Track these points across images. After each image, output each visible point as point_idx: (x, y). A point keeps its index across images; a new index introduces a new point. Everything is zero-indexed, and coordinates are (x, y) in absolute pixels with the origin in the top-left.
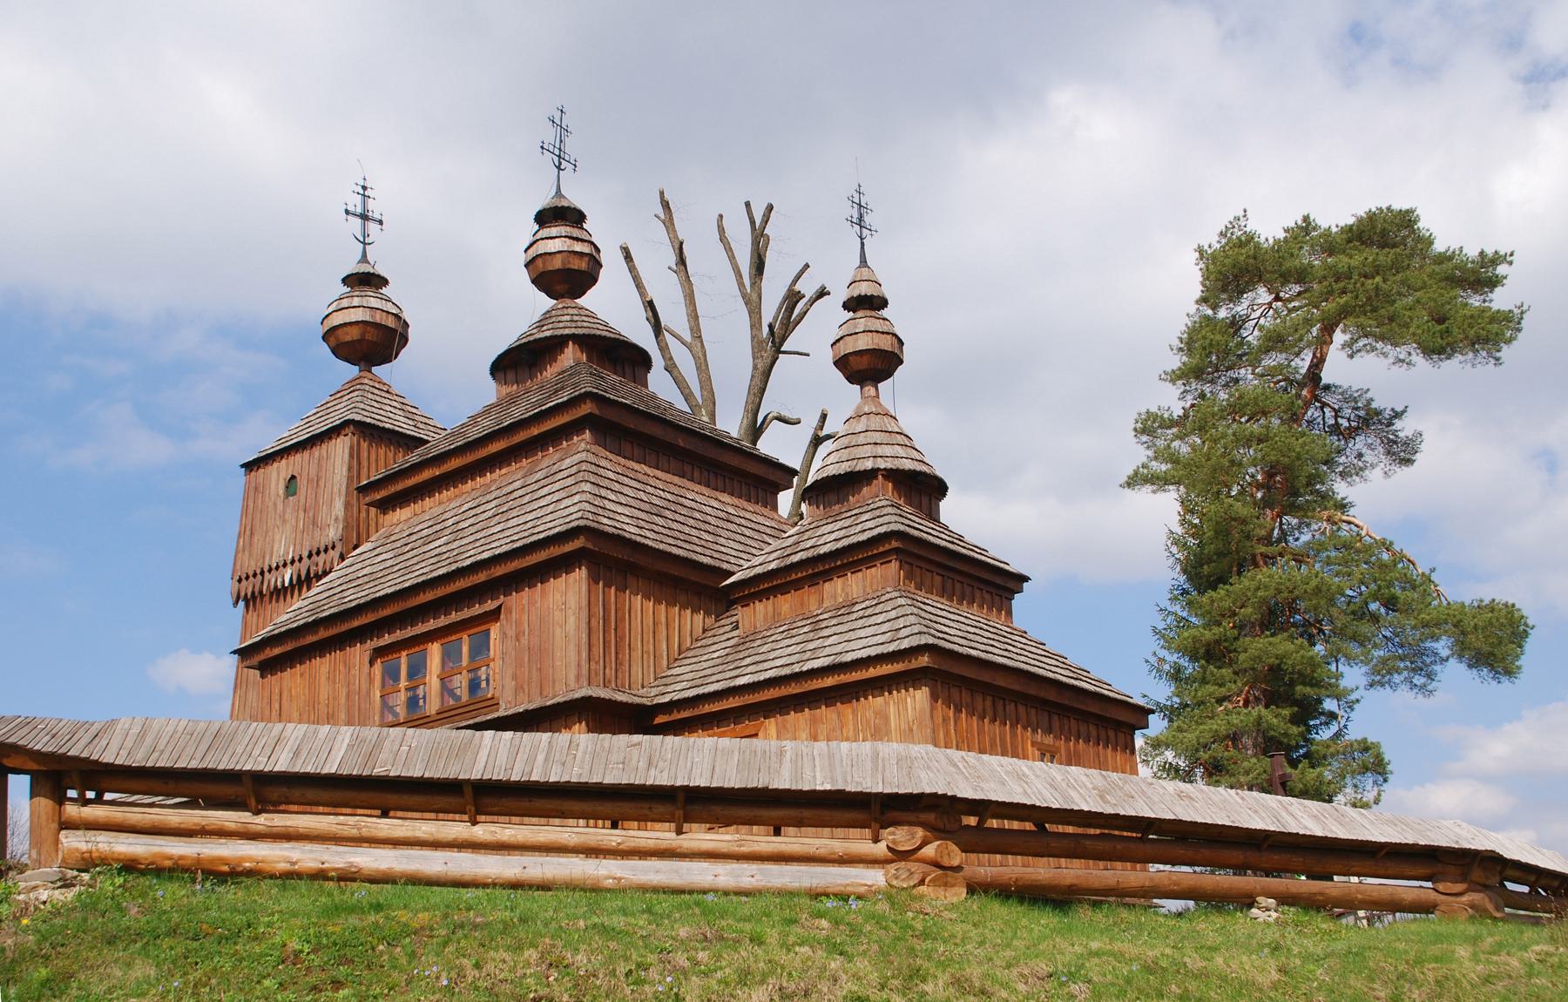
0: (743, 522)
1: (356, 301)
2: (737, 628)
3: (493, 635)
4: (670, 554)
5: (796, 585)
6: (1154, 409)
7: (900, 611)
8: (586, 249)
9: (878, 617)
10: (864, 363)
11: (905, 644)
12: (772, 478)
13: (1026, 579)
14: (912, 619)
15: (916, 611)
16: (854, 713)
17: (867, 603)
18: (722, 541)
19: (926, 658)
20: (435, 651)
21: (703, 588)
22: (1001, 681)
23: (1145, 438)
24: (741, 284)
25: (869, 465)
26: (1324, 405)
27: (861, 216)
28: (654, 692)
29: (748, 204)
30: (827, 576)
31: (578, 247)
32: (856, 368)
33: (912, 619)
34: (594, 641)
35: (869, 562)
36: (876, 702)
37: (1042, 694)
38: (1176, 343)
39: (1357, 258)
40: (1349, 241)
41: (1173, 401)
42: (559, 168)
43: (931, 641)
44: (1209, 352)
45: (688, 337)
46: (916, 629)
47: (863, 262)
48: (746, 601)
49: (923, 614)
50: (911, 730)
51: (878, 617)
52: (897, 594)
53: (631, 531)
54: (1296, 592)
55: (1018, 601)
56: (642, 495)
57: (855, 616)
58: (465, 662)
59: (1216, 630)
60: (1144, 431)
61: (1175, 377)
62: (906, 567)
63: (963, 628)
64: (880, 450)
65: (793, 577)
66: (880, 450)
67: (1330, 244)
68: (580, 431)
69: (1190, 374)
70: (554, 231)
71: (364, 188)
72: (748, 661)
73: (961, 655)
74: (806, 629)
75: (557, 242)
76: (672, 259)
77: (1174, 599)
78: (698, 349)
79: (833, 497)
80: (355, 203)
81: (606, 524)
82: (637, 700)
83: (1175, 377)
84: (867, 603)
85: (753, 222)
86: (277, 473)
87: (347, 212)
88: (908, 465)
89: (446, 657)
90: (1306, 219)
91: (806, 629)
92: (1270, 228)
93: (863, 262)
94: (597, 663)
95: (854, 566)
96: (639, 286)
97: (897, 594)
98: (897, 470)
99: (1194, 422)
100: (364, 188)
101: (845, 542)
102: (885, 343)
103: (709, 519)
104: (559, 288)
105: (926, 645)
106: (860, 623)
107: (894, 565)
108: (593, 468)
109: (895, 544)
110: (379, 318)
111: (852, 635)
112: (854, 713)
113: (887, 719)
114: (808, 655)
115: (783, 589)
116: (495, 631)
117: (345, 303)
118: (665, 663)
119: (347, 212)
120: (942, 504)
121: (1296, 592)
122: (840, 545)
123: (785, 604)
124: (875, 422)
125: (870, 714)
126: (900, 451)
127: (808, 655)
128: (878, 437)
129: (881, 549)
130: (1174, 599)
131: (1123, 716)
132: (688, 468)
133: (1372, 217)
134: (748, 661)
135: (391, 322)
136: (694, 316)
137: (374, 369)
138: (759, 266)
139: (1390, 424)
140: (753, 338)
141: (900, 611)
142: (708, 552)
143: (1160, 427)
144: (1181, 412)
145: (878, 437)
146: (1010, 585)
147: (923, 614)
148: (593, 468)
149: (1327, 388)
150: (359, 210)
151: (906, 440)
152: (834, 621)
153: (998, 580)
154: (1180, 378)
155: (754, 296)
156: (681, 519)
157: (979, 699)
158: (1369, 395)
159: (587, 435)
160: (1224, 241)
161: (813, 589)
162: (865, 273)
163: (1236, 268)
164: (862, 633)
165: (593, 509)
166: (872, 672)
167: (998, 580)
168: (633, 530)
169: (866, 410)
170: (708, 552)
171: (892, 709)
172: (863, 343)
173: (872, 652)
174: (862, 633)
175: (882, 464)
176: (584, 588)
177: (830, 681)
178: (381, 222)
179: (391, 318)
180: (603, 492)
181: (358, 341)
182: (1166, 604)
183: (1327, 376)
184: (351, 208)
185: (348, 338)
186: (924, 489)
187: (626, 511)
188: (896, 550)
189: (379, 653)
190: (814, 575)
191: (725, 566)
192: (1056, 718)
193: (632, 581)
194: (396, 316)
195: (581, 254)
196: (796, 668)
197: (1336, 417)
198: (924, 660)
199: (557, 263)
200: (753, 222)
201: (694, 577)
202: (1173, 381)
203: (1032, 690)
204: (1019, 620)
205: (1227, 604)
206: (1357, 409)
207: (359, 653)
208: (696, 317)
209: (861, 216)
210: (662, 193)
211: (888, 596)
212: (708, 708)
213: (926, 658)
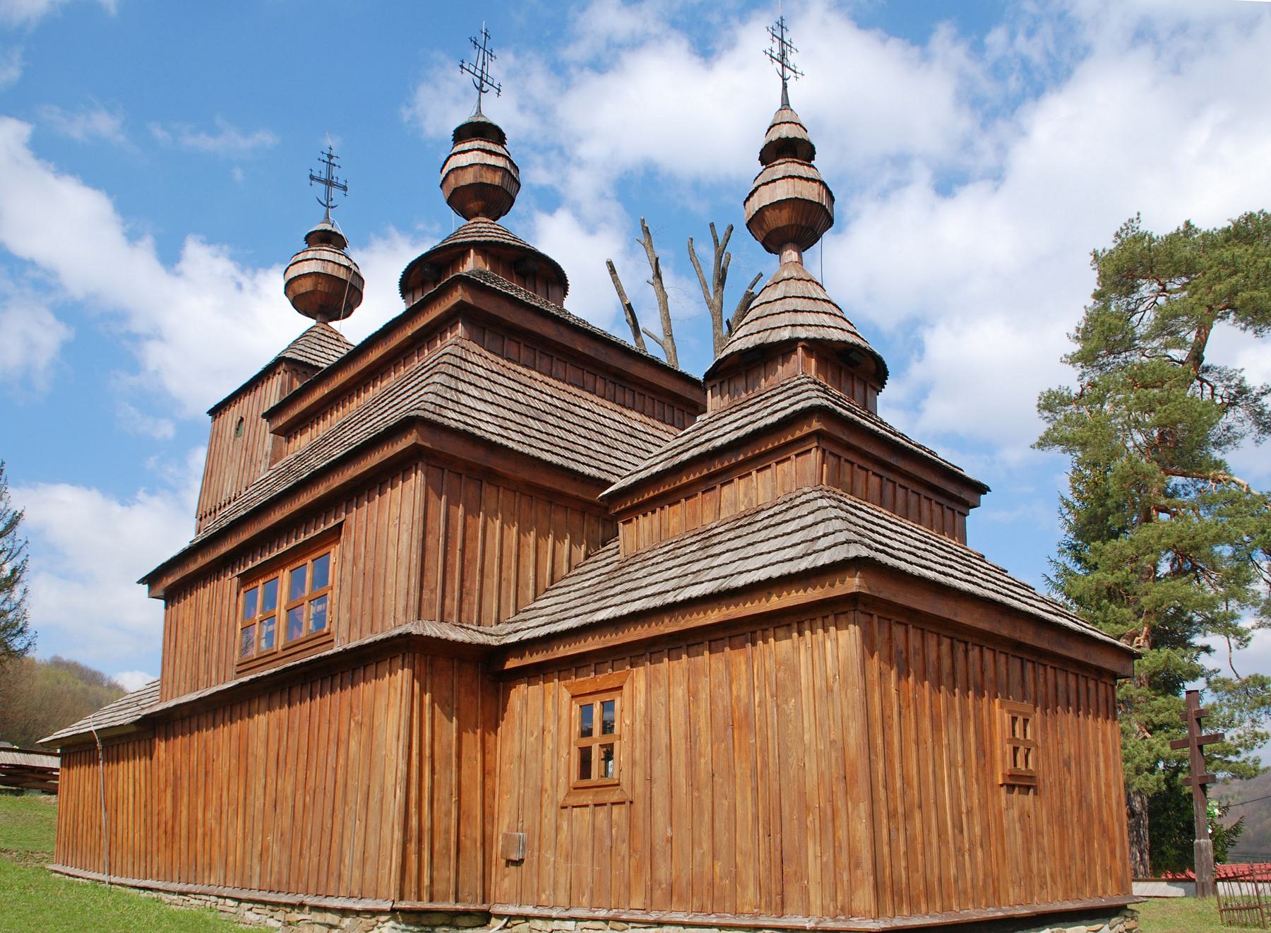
0: (651, 439)
1: (310, 255)
2: (618, 553)
3: (332, 560)
4: (539, 459)
5: (687, 492)
6: (1055, 389)
7: (820, 515)
8: (500, 162)
9: (791, 522)
10: (781, 219)
11: (825, 559)
12: (690, 396)
13: (981, 489)
14: (837, 524)
15: (843, 514)
16: (750, 662)
17: (776, 509)
18: (619, 454)
19: (857, 581)
20: (285, 576)
21: (587, 509)
22: (965, 616)
23: (1046, 414)
24: (706, 293)
25: (785, 334)
26: (1202, 381)
27: (783, 54)
28: (510, 628)
29: (712, 225)
30: (724, 477)
31: (492, 160)
32: (773, 225)
33: (837, 524)
34: (429, 563)
35: (780, 454)
36: (780, 648)
37: (1017, 635)
38: (1073, 332)
39: (1239, 250)
40: (1227, 241)
41: (1071, 380)
42: (480, 89)
43: (864, 552)
44: (1102, 338)
45: (660, 334)
46: (841, 537)
47: (785, 104)
48: (630, 514)
49: (853, 519)
50: (830, 690)
51: (791, 522)
52: (818, 494)
53: (489, 430)
54: (1198, 539)
55: (974, 519)
56: (520, 397)
57: (759, 525)
58: (307, 593)
59: (1118, 574)
60: (1045, 408)
61: (1073, 359)
62: (831, 459)
63: (908, 545)
64: (800, 318)
65: (685, 480)
66: (800, 318)
67: (1210, 241)
68: (453, 327)
69: (1085, 358)
70: (467, 146)
71: (330, 157)
72: (618, 589)
73: (911, 575)
74: (694, 548)
75: (472, 156)
76: (650, 273)
77: (1062, 552)
78: (669, 345)
79: (741, 384)
80: (321, 170)
81: (452, 418)
82: (481, 639)
83: (1073, 359)
84: (776, 509)
85: (716, 241)
86: (232, 415)
87: (312, 178)
88: (836, 335)
89: (297, 584)
90: (1188, 223)
91: (694, 548)
92: (1161, 225)
93: (785, 104)
94: (433, 591)
95: (760, 462)
96: (621, 293)
97: (818, 494)
98: (823, 340)
99: (1093, 396)
100: (330, 157)
101: (749, 429)
102: (811, 192)
103: (607, 431)
104: (473, 206)
105: (857, 559)
106: (763, 535)
107: (815, 456)
108: (457, 362)
109: (816, 425)
110: (330, 269)
111: (751, 551)
112: (750, 662)
113: (795, 673)
114: (689, 579)
115: (670, 499)
116: (335, 553)
117: (300, 257)
118: (531, 593)
119: (312, 178)
120: (880, 398)
121: (1198, 539)
122: (742, 433)
123: (674, 517)
124: (796, 288)
125: (770, 664)
126: (827, 320)
127: (689, 579)
128: (799, 304)
129: (798, 434)
130: (1062, 552)
131: (1109, 663)
132: (589, 379)
133: (1250, 217)
134: (618, 589)
135: (342, 274)
136: (667, 319)
137: (334, 324)
138: (721, 279)
139: (1256, 400)
140: (715, 335)
141: (820, 515)
142: (593, 463)
143: (1060, 404)
144: (1079, 390)
145: (799, 304)
146: (966, 495)
147: (853, 519)
148: (457, 362)
149: (1206, 369)
150: (324, 176)
151: (836, 311)
152: (731, 535)
153: (952, 489)
154: (1079, 359)
155: (717, 302)
156: (568, 426)
157: (932, 641)
158: (1242, 374)
159: (460, 329)
160: (1119, 241)
161: (708, 496)
162: (787, 116)
163: (1132, 265)
164: (764, 547)
165: (439, 401)
166: (776, 602)
167: (952, 489)
168: (491, 428)
169: (786, 275)
170: (593, 463)
171: (803, 657)
172: (782, 191)
173: (775, 572)
174: (764, 547)
175: (802, 333)
176: (419, 496)
177: (714, 616)
178: (345, 189)
179: (342, 269)
180: (462, 386)
181: (312, 292)
182: (1054, 556)
183: (1209, 357)
184: (316, 174)
185: (302, 290)
186: (857, 366)
187: (490, 409)
188: (818, 434)
189: (247, 579)
190: (711, 477)
191: (603, 476)
192: (1029, 666)
193: (489, 493)
194: (348, 268)
195: (494, 168)
196: (670, 598)
197: (1213, 394)
198: (853, 584)
199: (468, 178)
200: (716, 241)
201: (571, 489)
202: (1073, 363)
203: (1004, 629)
204: (975, 542)
205: (1130, 551)
206: (1230, 387)
207: (229, 582)
208: (669, 320)
209: (783, 54)
210: (643, 221)
211: (804, 498)
212: (563, 651)
213: (857, 581)
